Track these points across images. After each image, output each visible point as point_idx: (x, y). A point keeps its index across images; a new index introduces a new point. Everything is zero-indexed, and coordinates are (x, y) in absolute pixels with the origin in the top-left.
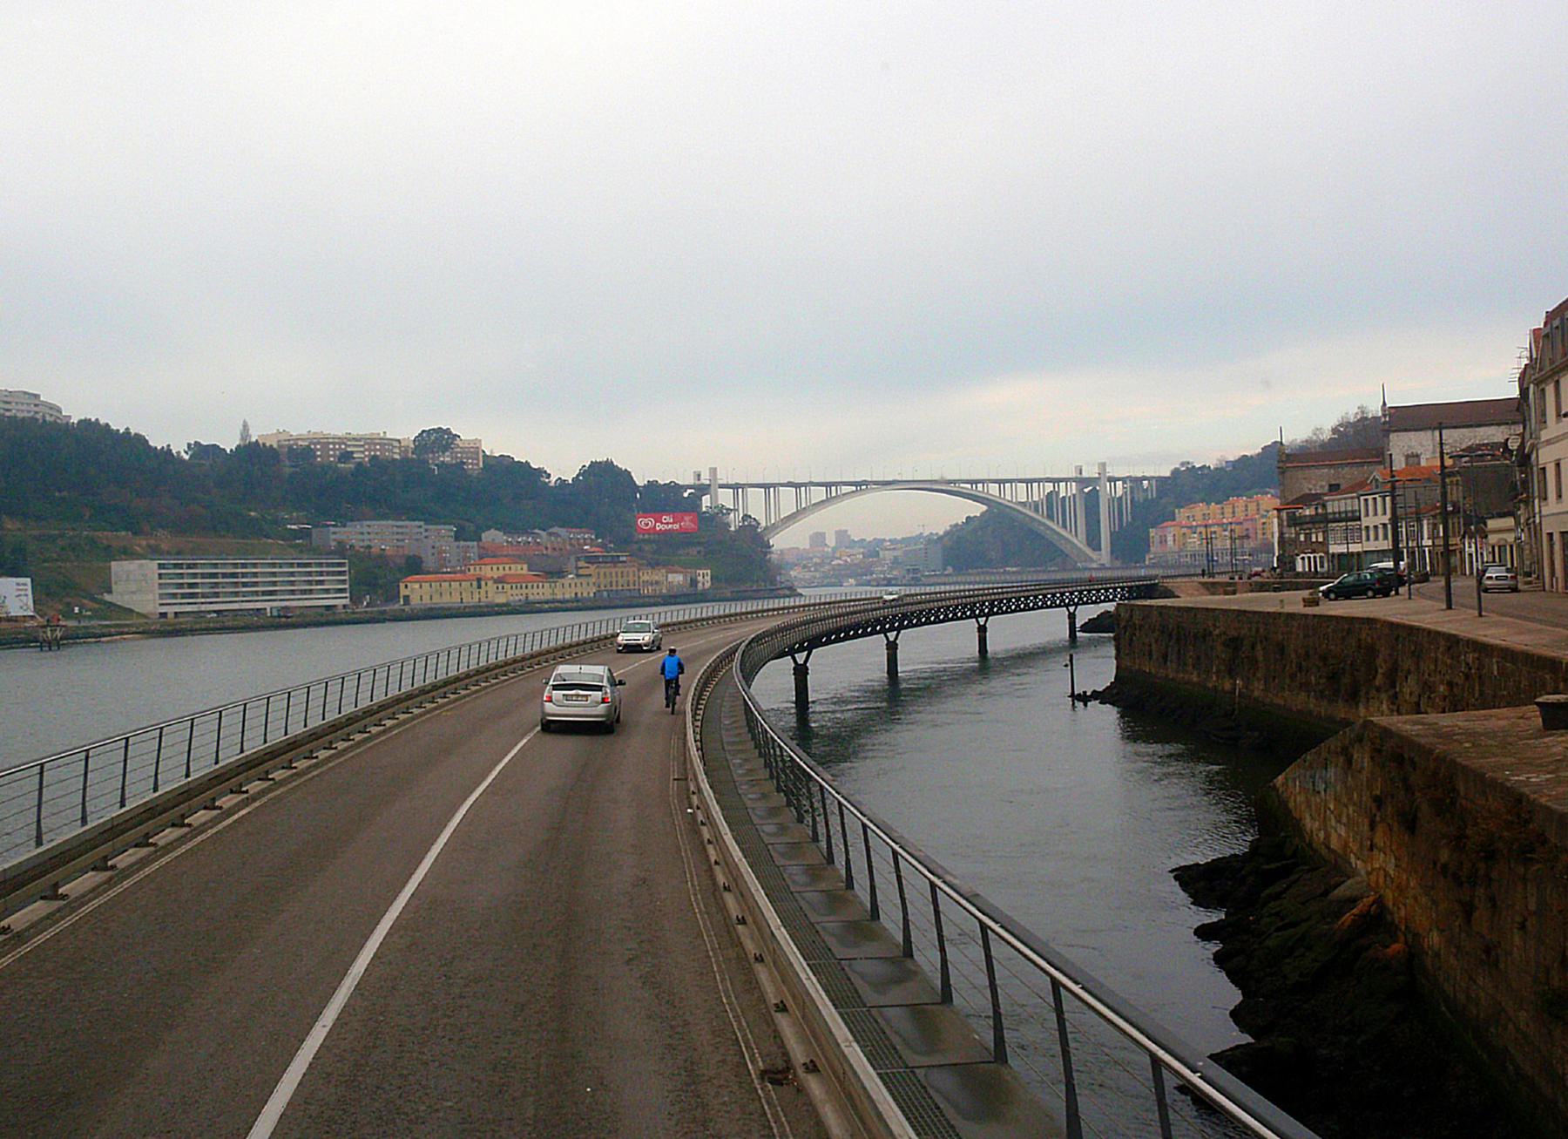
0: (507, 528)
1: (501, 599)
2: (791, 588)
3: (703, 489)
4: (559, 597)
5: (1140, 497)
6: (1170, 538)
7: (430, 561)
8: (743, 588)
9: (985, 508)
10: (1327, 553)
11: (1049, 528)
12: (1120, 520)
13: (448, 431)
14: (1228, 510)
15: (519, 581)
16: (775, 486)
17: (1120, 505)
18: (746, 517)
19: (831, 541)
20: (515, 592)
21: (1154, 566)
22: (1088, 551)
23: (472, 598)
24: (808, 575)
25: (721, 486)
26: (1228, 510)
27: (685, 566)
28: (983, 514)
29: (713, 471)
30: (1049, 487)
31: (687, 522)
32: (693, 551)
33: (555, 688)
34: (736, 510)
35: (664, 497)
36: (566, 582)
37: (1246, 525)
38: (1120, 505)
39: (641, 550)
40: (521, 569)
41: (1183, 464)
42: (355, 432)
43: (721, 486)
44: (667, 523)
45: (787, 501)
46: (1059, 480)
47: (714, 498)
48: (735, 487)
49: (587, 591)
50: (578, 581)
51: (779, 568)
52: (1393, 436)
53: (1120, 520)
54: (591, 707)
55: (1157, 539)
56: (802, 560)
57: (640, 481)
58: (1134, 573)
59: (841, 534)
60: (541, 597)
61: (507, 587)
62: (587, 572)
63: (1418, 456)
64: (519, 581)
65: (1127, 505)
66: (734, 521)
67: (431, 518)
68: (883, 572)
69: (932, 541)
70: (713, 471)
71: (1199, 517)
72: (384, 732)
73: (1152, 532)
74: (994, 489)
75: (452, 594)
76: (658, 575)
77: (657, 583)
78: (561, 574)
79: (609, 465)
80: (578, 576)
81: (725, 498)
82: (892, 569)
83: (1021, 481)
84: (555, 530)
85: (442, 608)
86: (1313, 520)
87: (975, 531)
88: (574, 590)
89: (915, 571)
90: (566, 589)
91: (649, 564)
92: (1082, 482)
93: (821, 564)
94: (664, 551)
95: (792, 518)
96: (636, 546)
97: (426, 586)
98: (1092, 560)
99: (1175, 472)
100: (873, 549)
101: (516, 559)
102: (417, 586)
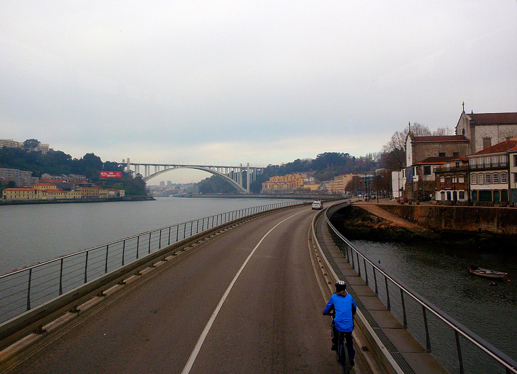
0: (52, 173)
1: (44, 198)
2: (152, 197)
3: (125, 165)
4: (68, 198)
6: (268, 186)
7: (19, 184)
9: (212, 175)
10: (468, 190)
13: (36, 140)
14: (286, 178)
15: (52, 192)
16: (148, 165)
18: (139, 174)
19: (166, 184)
20: (50, 195)
21: (262, 194)
22: (243, 189)
23: (32, 197)
24: (159, 193)
25: (131, 164)
26: (286, 178)
27: (115, 189)
29: (129, 159)
30: (232, 169)
31: (118, 175)
35: (111, 166)
36: (71, 193)
39: (101, 183)
40: (55, 188)
43: (131, 164)
44: (111, 175)
45: (152, 170)
46: (235, 168)
48: (135, 165)
49: (79, 196)
50: (75, 193)
51: (149, 191)
52: (477, 128)
55: (264, 187)
56: (157, 189)
57: (103, 161)
59: (169, 182)
60: (61, 198)
61: (47, 194)
62: (78, 189)
63: (490, 139)
64: (52, 192)
66: (134, 175)
67: (22, 168)
69: (195, 184)
70: (129, 159)
73: (263, 184)
74: (216, 169)
75: (24, 195)
76: (105, 191)
78: (69, 190)
79: (93, 155)
80: (76, 191)
81: (132, 168)
82: (183, 192)
83: (224, 167)
84: (71, 175)
85: (22, 201)
86: (454, 171)
88: (73, 196)
89: (191, 193)
90: (70, 195)
92: (242, 168)
93: (163, 190)
94: (109, 184)
95: (153, 175)
97: (13, 192)
100: (178, 187)
101: (54, 184)
102: (10, 192)
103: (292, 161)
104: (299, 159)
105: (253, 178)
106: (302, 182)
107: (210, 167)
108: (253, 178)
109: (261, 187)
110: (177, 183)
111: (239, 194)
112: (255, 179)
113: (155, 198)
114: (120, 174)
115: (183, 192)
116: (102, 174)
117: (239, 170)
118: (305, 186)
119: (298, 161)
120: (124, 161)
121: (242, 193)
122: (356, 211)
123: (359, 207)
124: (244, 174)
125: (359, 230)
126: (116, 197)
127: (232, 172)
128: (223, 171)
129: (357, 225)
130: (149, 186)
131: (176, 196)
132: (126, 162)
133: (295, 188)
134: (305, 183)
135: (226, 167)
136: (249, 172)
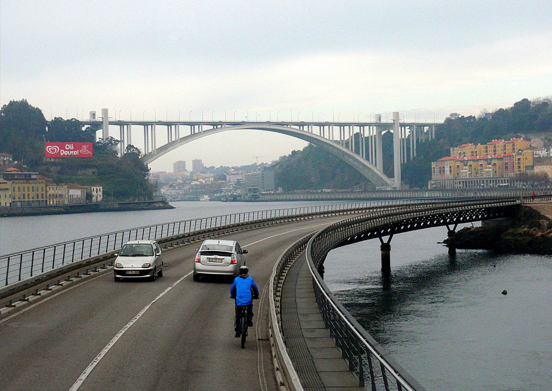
2: (163, 202)
3: (96, 125)
5: (423, 138)
6: (447, 169)
8: (127, 201)
11: (355, 159)
12: (408, 156)
17: (408, 144)
18: (130, 146)
19: (189, 168)
25: (112, 123)
26: (491, 148)
27: (82, 183)
28: (305, 149)
29: (105, 111)
30: (357, 129)
31: (85, 150)
32: (90, 171)
33: (203, 253)
34: (122, 141)
35: (68, 130)
37: (506, 160)
38: (408, 144)
39: (48, 170)
41: (452, 115)
42: (518, 101)
43: (112, 123)
44: (69, 150)
45: (161, 136)
47: (105, 132)
48: (121, 124)
51: (156, 186)
53: (408, 156)
54: (225, 266)
55: (437, 170)
57: (49, 117)
58: (418, 194)
59: (197, 163)
65: (413, 146)
66: (121, 150)
68: (228, 191)
69: (265, 168)
70: (105, 111)
71: (468, 154)
72: (88, 278)
74: (316, 130)
76: (61, 190)
77: (61, 196)
81: (114, 132)
83: (160, 123)
87: (299, 161)
89: (255, 190)
91: (54, 181)
92: (380, 126)
94: (66, 172)
95: (164, 149)
96: (45, 167)
98: (388, 185)
99: (448, 121)
100: (222, 174)
103: (508, 103)
104: (525, 100)
105: (408, 149)
106: (530, 158)
107: (302, 124)
108: (408, 149)
109: (428, 172)
110: (217, 166)
111: (375, 191)
112: (413, 153)
113: (171, 204)
114: (88, 149)
115: (235, 188)
116: (49, 149)
117: (374, 131)
118: (538, 169)
119: (523, 106)
120: (94, 115)
121: (383, 188)
122: (525, 214)
123: (529, 207)
124: (387, 141)
125: (518, 241)
126: (83, 202)
127: (357, 135)
128: (335, 135)
129: (520, 234)
130: (157, 175)
131: (219, 199)
132: (98, 118)
133: (512, 175)
134: (539, 161)
135: (341, 125)
136: (401, 135)
